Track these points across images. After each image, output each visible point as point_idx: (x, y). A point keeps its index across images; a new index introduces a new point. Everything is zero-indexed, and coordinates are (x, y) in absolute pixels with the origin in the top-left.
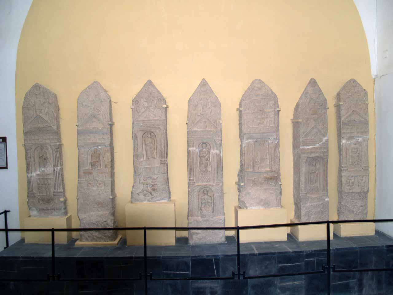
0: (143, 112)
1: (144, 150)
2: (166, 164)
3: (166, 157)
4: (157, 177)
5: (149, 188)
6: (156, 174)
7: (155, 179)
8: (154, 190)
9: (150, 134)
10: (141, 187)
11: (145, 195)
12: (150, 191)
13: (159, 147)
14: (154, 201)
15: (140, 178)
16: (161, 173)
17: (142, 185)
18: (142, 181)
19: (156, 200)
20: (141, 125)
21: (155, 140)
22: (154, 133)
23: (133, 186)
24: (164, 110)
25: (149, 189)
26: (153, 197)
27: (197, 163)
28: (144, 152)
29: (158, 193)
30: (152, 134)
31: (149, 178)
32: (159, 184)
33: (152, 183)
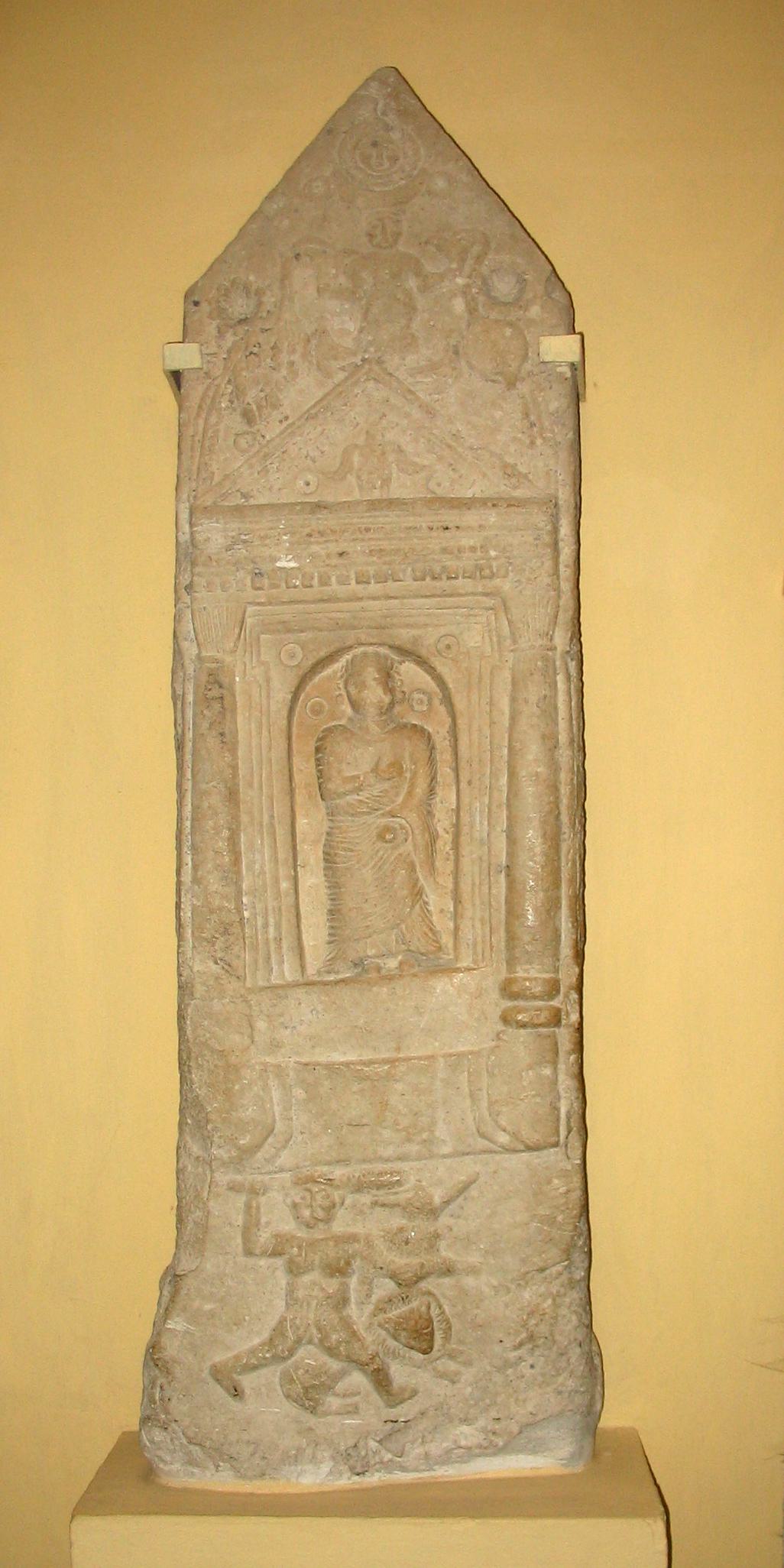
0: (310, 416)
1: (312, 855)
2: (565, 1037)
3: (566, 950)
4: (466, 1187)
5: (358, 1314)
6: (446, 1150)
7: (433, 1213)
8: (421, 1335)
9: (387, 677)
10: (268, 1297)
11: (309, 1396)
12: (373, 1339)
13: (484, 828)
14: (409, 1459)
15: (254, 1191)
16: (504, 1138)
17: (282, 1279)
18: (278, 1217)
19: (435, 1448)
20: (286, 563)
21: (442, 742)
22: (431, 670)
23: (173, 1278)
24: (556, 401)
25: (360, 1327)
26: (402, 1412)
27: (199, 630)
28: (313, 880)
29: (468, 1375)
30: (409, 672)
31: (366, 1199)
32: (473, 1271)
33: (400, 1261)
